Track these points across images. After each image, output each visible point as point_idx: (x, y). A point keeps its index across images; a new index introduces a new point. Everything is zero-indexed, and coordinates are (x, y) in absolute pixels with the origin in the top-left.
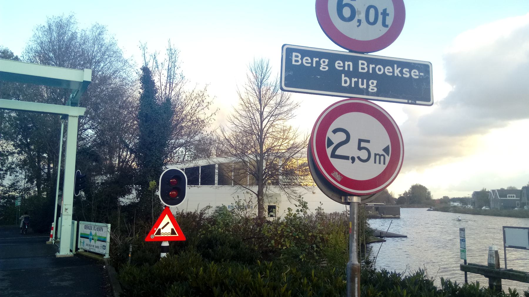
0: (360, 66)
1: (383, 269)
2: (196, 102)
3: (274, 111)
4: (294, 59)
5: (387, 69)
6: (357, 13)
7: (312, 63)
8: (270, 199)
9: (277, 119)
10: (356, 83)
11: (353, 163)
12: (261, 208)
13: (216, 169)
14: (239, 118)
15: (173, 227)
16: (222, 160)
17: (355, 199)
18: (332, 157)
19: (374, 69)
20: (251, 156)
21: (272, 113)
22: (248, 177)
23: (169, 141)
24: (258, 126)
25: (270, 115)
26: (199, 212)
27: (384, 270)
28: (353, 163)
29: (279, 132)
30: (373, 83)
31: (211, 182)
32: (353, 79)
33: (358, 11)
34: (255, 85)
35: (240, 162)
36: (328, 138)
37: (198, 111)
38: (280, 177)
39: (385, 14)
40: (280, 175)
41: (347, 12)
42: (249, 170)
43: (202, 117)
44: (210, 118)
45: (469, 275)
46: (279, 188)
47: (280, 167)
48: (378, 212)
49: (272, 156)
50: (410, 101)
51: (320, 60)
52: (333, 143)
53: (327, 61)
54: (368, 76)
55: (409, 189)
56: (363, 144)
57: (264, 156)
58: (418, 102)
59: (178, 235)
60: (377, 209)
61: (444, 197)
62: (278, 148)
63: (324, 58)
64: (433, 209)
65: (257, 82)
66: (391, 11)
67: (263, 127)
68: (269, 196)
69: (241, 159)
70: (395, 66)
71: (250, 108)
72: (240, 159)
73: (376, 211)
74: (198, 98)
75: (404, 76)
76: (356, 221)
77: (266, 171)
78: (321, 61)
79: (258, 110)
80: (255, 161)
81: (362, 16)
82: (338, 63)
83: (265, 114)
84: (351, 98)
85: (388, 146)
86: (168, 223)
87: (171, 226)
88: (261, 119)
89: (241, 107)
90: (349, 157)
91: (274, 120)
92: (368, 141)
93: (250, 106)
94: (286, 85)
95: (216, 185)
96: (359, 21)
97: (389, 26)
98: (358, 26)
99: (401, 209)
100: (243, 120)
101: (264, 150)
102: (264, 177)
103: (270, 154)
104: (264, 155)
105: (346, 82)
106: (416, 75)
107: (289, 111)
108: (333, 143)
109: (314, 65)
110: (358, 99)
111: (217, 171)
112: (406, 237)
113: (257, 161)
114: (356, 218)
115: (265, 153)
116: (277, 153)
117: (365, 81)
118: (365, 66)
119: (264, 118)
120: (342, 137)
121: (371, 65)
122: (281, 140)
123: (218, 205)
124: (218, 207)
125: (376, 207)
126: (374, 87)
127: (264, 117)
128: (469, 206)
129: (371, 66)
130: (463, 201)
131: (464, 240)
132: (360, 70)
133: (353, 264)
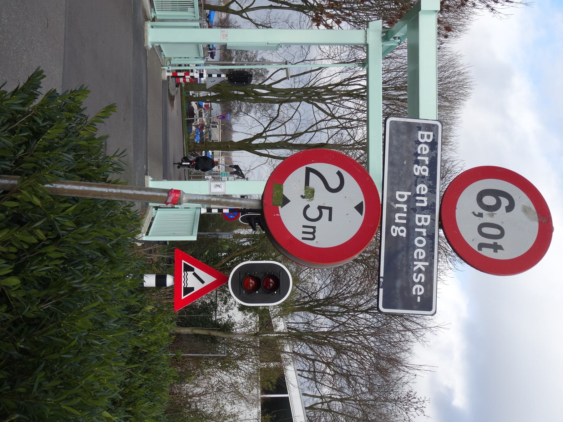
6: (490, 212)
10: (400, 210)
15: (195, 290)
19: (420, 234)
23: (334, 297)
30: (402, 231)
41: (489, 200)
54: (410, 226)
56: (326, 212)
59: (183, 260)
63: (429, 170)
66: (500, 256)
70: (427, 264)
75: (415, 275)
81: (487, 218)
86: (203, 282)
87: (197, 286)
92: (330, 219)
96: (480, 215)
97: (480, 252)
98: (474, 213)
117: (405, 221)
118: (423, 223)
129: (424, 231)
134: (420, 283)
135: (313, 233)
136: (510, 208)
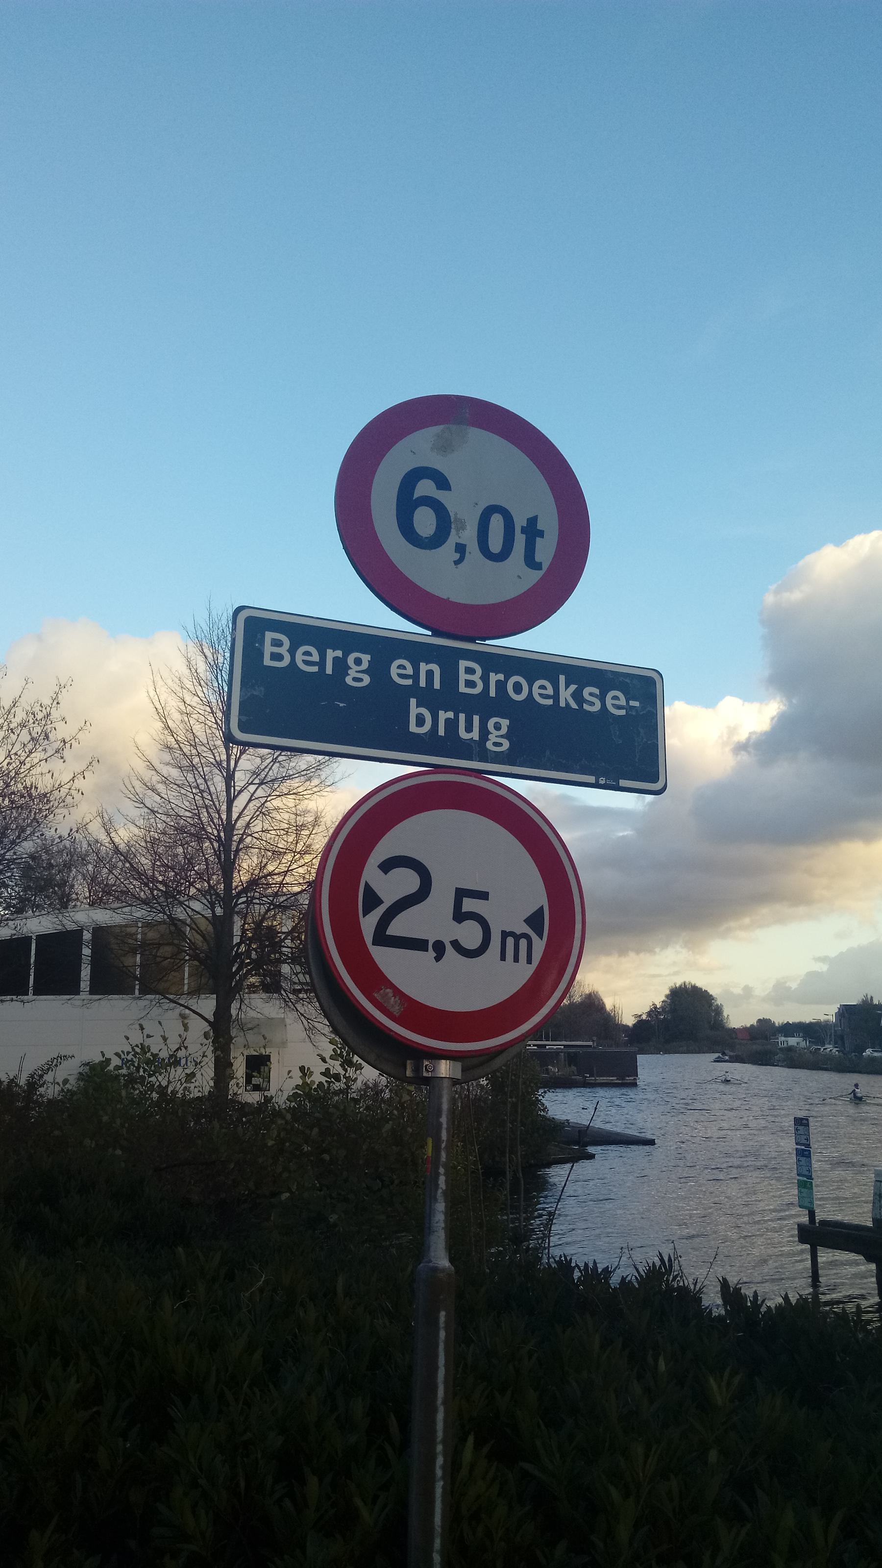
0: (463, 677)
1: (561, 1256)
2: (25, 737)
3: (267, 770)
4: (268, 649)
5: (303, 654)
6: (453, 526)
7: (322, 664)
8: (250, 1036)
9: (278, 793)
10: (452, 725)
11: (438, 959)
12: (223, 1067)
13: (84, 946)
14: (161, 788)
16: (102, 917)
17: (444, 1068)
18: (375, 943)
19: (501, 686)
20: (196, 906)
21: (263, 775)
22: (187, 969)
24: (218, 812)
25: (257, 781)
26: (22, 1081)
27: (563, 1258)
28: (438, 959)
29: (282, 832)
30: (498, 727)
31: (70, 987)
32: (441, 713)
33: (456, 519)
34: (211, 691)
35: (164, 922)
36: (367, 884)
37: (28, 766)
38: (286, 969)
39: (532, 531)
40: (284, 962)
42: (190, 948)
43: (44, 784)
44: (67, 786)
45: (825, 1256)
46: (278, 1002)
47: (285, 938)
48: (574, 1068)
49: (260, 904)
50: (602, 781)
51: (346, 655)
52: (379, 902)
53: (366, 658)
55: (663, 998)
56: (469, 905)
57: (236, 905)
58: (623, 783)
60: (572, 1058)
61: (759, 1021)
62: (279, 879)
64: (730, 1057)
65: (218, 681)
66: (549, 523)
67: (235, 816)
68: (249, 1026)
69: (165, 913)
70: (562, 678)
71: (196, 760)
72: (161, 912)
73: (570, 1065)
74: (32, 725)
76: (444, 1135)
77: (243, 948)
78: (350, 660)
79: (219, 764)
80: (206, 918)
81: (469, 535)
82: (399, 667)
83: (240, 779)
84: (438, 768)
85: (541, 909)
88: (228, 788)
89: (167, 757)
90: (427, 941)
91: (267, 797)
93: (194, 751)
94: (244, 727)
95: (85, 996)
97: (545, 566)
98: (457, 563)
99: (641, 1058)
100: (172, 795)
101: (234, 884)
102: (234, 969)
103: (253, 898)
104: (237, 901)
105: (420, 721)
106: (619, 707)
107: (313, 770)
108: (379, 902)
109: (329, 670)
110: (449, 770)
111: (86, 951)
112: (651, 1142)
113: (215, 920)
114: (445, 1126)
115: (239, 896)
116: (276, 895)
117: (476, 719)
118: (476, 678)
119: (238, 788)
120: (408, 881)
121: (492, 675)
122: (289, 857)
123: (86, 1059)
124: (88, 1064)
125: (569, 1053)
126: (502, 736)
127: (236, 788)
128: (829, 1047)
129: (494, 678)
130: (810, 1031)
131: (806, 1150)
132: (462, 689)
133: (435, 1269)
134: (602, 698)
135: (517, 938)
136: (443, 483)
